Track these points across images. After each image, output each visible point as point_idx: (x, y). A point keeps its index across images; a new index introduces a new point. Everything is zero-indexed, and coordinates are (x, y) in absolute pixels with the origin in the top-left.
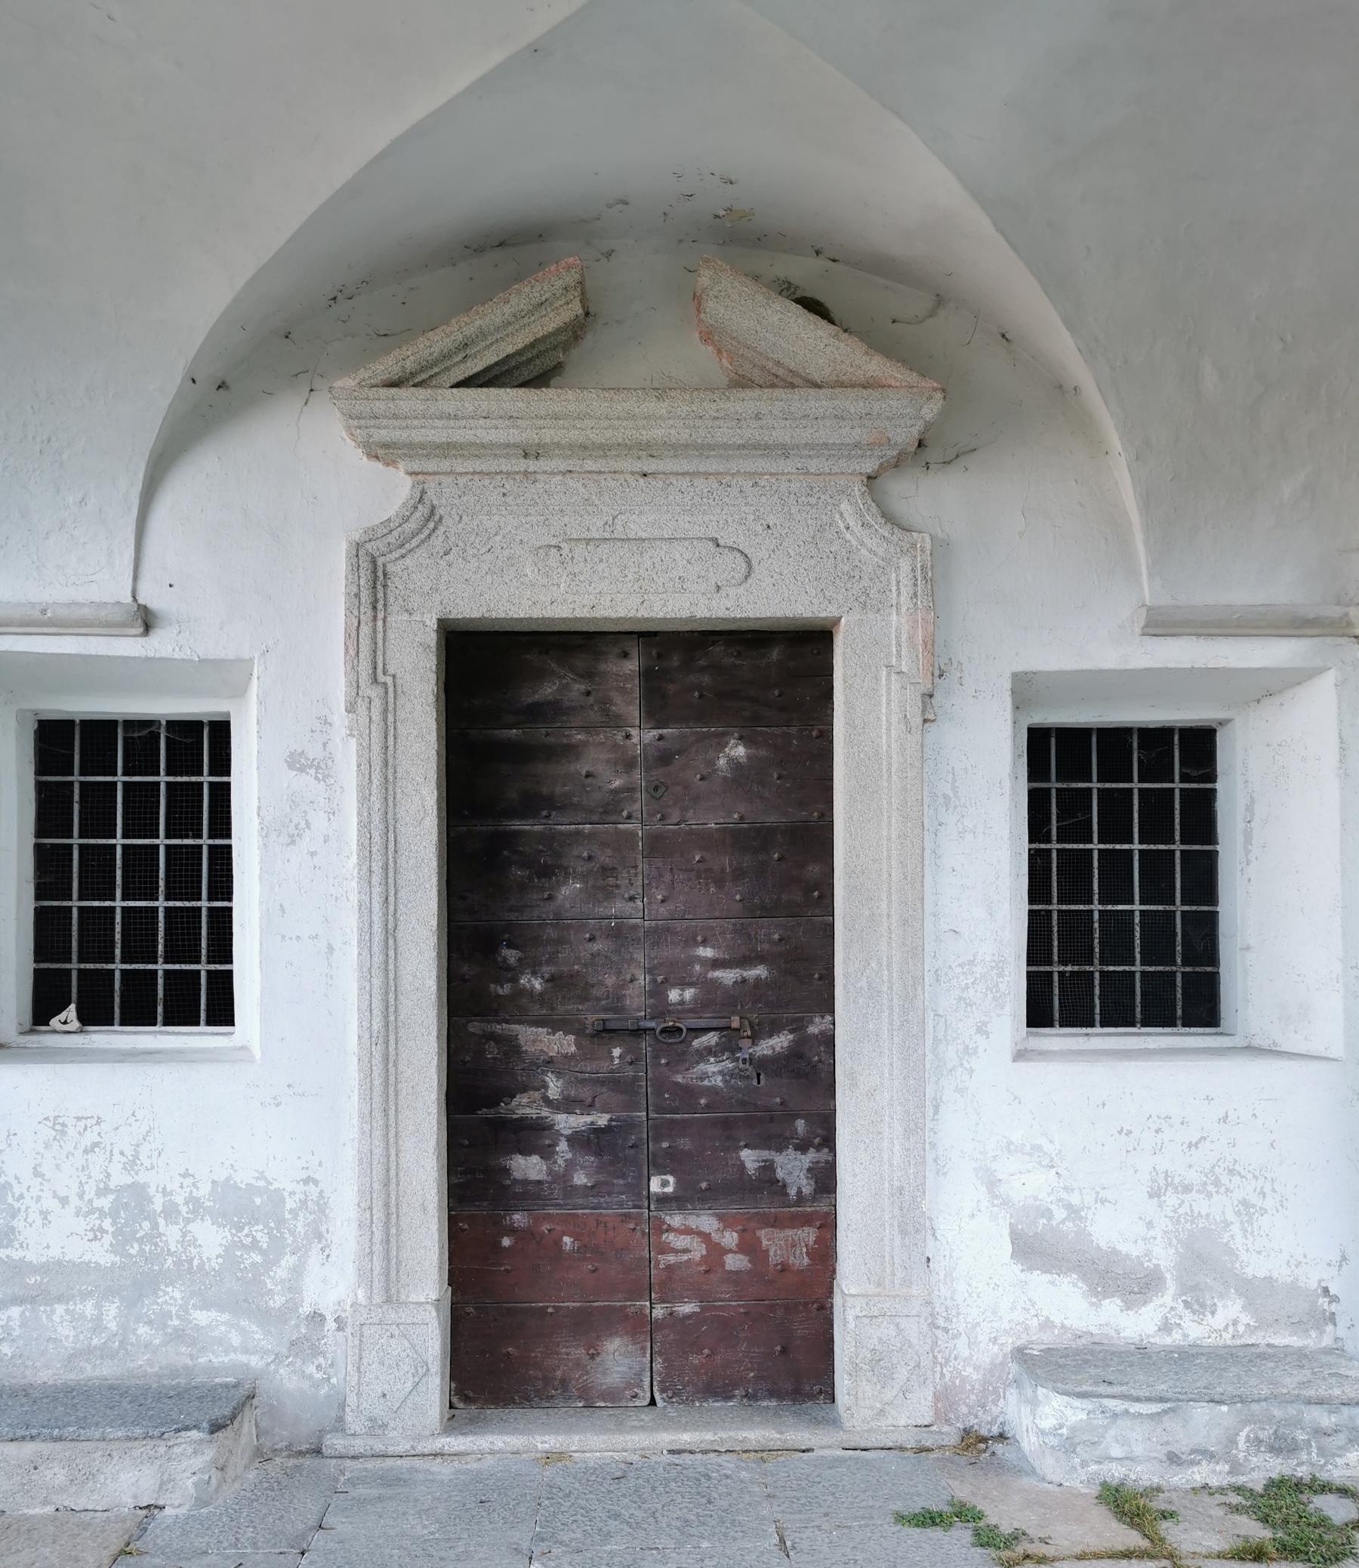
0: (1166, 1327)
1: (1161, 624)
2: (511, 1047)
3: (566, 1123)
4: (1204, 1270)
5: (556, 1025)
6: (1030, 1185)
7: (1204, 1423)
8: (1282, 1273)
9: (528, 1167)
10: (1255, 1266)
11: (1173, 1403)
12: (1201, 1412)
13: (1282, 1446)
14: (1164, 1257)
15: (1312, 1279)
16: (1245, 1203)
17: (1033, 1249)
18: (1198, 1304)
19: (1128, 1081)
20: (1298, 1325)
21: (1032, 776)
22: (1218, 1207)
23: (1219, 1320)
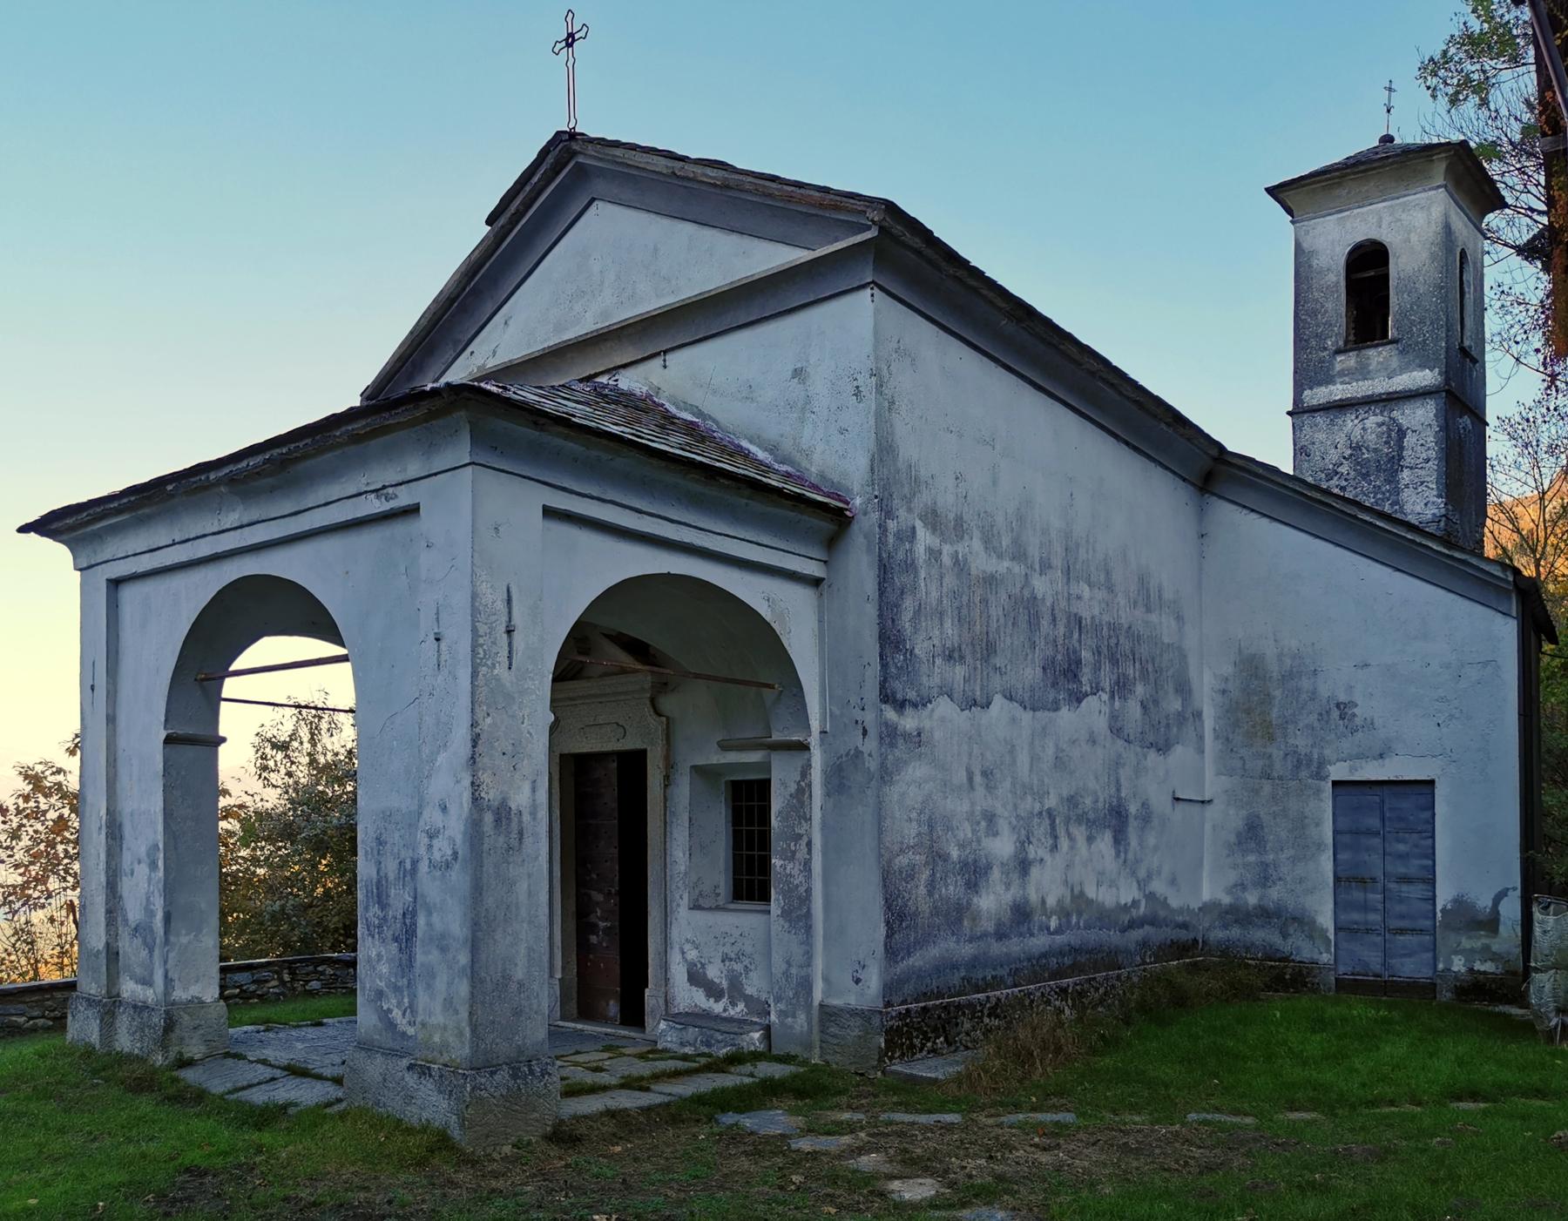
0: (725, 1010)
1: (725, 746)
2: (589, 896)
3: (602, 924)
4: (735, 990)
5: (600, 891)
6: (692, 955)
7: (692, 1032)
8: (755, 994)
9: (594, 939)
10: (749, 991)
11: (686, 1025)
12: (691, 1029)
13: (709, 1045)
14: (725, 984)
15: (763, 997)
16: (1128, 1024)
17: (696, 977)
18: (734, 1004)
19: (744, 922)
20: (759, 1015)
21: (734, 800)
22: (738, 967)
23: (738, 1009)
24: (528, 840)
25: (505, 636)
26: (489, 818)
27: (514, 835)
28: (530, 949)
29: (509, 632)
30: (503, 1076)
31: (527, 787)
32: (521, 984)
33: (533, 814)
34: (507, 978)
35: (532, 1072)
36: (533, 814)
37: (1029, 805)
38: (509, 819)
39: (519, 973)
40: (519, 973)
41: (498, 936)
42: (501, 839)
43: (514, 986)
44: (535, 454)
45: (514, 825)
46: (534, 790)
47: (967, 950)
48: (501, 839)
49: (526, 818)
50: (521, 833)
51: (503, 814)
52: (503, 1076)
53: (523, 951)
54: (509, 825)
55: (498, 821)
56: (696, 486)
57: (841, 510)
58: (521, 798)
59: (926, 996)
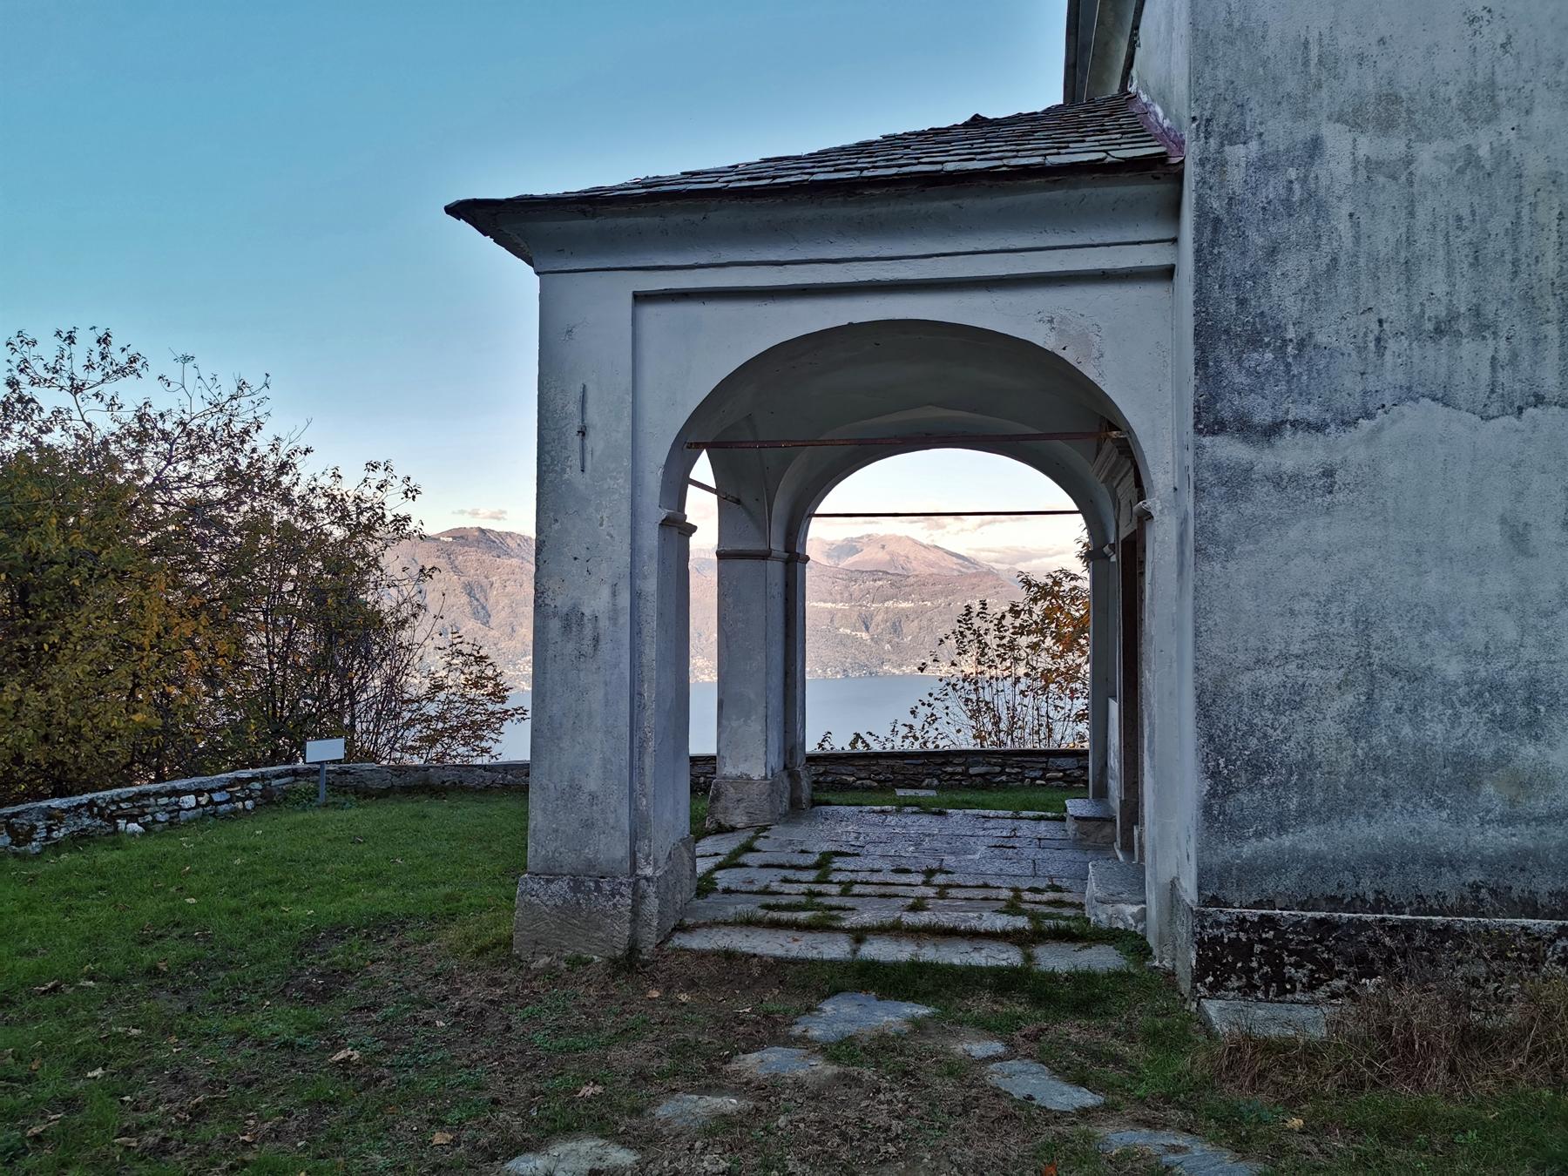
24: (605, 646)
25: (578, 439)
26: (555, 625)
27: (588, 641)
28: (606, 761)
29: (583, 433)
30: (561, 886)
31: (605, 592)
32: (593, 797)
33: (614, 619)
34: (575, 788)
35: (598, 888)
36: (614, 619)
37: (325, 481)
38: (580, 624)
39: (592, 784)
40: (592, 784)
41: (565, 744)
42: (570, 646)
43: (585, 798)
44: (609, 242)
45: (588, 631)
46: (614, 594)
47: (1495, 839)
48: (570, 646)
49: (604, 623)
50: (596, 640)
51: (572, 620)
52: (561, 886)
53: (597, 758)
54: (581, 631)
55: (567, 627)
56: (808, 212)
57: (1161, 159)
58: (597, 602)
59: (1334, 902)
